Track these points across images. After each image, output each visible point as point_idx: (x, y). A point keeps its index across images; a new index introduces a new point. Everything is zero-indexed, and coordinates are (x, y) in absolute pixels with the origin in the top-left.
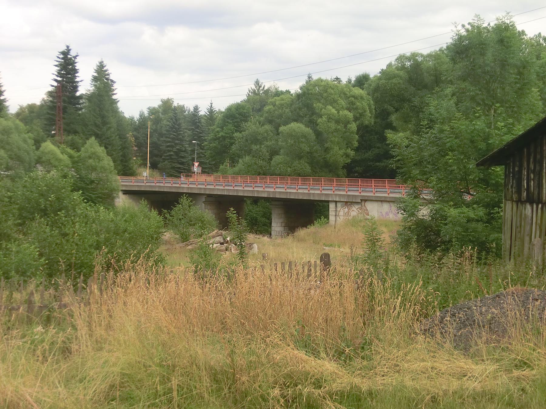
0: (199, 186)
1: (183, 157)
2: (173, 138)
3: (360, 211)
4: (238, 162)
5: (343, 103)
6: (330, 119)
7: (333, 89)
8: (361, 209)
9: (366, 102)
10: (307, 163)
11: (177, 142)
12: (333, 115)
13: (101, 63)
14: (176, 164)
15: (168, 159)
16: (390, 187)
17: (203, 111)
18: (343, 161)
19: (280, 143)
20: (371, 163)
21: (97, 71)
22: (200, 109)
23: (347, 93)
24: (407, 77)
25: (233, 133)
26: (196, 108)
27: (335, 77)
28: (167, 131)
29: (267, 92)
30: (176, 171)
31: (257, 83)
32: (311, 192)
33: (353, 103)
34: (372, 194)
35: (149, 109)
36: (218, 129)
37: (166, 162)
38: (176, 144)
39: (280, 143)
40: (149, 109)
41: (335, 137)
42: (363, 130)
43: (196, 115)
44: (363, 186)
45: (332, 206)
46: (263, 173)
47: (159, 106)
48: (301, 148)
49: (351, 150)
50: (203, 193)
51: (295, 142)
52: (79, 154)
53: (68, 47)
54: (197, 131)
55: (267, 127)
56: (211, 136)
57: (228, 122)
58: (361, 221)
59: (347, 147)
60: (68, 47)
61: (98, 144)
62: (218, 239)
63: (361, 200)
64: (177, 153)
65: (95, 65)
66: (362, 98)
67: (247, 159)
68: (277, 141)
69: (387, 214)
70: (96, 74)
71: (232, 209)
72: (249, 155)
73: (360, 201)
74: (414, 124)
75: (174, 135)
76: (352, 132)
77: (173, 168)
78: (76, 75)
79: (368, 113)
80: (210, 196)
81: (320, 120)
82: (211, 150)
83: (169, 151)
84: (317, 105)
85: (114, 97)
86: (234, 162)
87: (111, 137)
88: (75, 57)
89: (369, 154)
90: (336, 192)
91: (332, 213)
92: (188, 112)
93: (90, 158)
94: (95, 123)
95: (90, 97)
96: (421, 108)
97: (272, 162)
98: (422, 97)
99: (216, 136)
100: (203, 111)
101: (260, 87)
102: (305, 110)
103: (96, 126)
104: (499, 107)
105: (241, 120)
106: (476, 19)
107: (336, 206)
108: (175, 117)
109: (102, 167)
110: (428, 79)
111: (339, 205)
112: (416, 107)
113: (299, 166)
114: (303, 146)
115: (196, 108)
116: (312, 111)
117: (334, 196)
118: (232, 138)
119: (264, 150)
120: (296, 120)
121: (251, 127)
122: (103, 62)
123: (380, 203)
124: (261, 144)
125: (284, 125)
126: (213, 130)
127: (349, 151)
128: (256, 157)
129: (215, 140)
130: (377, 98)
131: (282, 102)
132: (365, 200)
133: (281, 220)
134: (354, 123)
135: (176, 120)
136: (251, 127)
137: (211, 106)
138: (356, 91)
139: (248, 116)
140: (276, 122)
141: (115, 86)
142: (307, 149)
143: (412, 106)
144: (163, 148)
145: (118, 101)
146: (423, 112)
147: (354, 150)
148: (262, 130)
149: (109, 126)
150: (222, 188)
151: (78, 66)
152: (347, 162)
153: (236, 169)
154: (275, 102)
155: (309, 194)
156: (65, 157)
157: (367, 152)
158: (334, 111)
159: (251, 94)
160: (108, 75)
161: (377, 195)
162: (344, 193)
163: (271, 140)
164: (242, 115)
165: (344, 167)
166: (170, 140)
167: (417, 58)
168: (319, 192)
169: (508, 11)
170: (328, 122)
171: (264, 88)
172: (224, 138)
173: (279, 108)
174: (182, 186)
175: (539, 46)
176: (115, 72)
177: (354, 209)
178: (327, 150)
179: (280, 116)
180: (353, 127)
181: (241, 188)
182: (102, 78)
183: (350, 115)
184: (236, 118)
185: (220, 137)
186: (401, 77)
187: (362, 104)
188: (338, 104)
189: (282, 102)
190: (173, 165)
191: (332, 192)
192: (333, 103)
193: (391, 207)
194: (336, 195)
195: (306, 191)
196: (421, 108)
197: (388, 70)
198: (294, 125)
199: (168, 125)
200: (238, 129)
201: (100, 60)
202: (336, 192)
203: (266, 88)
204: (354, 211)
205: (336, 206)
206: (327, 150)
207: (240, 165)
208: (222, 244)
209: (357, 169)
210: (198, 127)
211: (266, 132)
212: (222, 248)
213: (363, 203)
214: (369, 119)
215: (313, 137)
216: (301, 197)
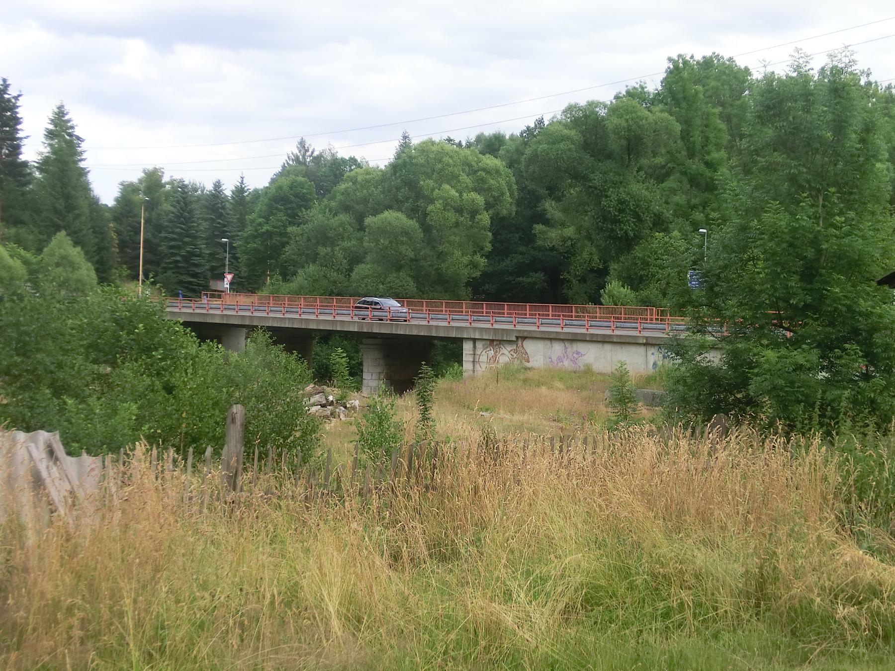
0: (241, 313)
1: (196, 265)
2: (180, 234)
3: (515, 355)
4: (295, 274)
5: (468, 181)
6: (446, 206)
7: (451, 157)
8: (516, 351)
9: (504, 182)
10: (410, 276)
11: (187, 239)
12: (452, 199)
13: (60, 108)
14: (184, 277)
15: (172, 268)
16: (473, 312)
17: (228, 191)
18: (465, 273)
19: (366, 244)
20: (511, 278)
21: (53, 121)
22: (223, 187)
23: (474, 164)
24: (582, 139)
25: (285, 227)
26: (218, 185)
27: (445, 138)
28: (170, 221)
29: (318, 159)
30: (185, 287)
31: (302, 144)
32: (432, 323)
33: (483, 180)
34: (534, 328)
35: (122, 184)
36: (261, 220)
37: (169, 273)
38: (187, 243)
39: (366, 244)
40: (122, 184)
41: (454, 234)
42: (500, 224)
43: (217, 197)
44: (433, 311)
45: (467, 347)
46: (334, 292)
47: (140, 181)
48: (400, 253)
49: (481, 257)
50: (247, 323)
51: (391, 242)
52: (39, 258)
53: (4, 80)
54: (219, 223)
55: (343, 217)
56: (249, 230)
57: (277, 209)
58: (518, 371)
59: (475, 252)
60: (4, 80)
61: (70, 242)
62: (317, 398)
63: (517, 338)
64: (187, 259)
65: (51, 111)
66: (498, 172)
67: (312, 268)
68: (361, 240)
69: (560, 360)
70: (51, 127)
71: (340, 350)
72: (314, 262)
73: (514, 339)
74: (593, 217)
75: (182, 228)
76: (484, 228)
77: (180, 283)
78: (19, 127)
79: (507, 197)
80: (270, 329)
81: (430, 208)
82: (247, 254)
83: (174, 255)
84: (426, 183)
85: (82, 165)
86: (286, 275)
87: (81, 230)
88: (16, 98)
89: (508, 263)
90: (474, 325)
91: (467, 357)
92: (202, 191)
93: (58, 265)
94: (54, 208)
95: (44, 165)
96: (605, 190)
97: (353, 275)
98: (605, 173)
99: (257, 231)
100: (228, 191)
101: (307, 151)
102: (405, 190)
103: (56, 211)
104: (834, 193)
105: (300, 207)
106: (796, 55)
107: (475, 347)
108: (184, 198)
109: (79, 281)
110: (615, 144)
111: (479, 345)
112: (596, 188)
113: (398, 281)
114: (403, 249)
115: (218, 185)
116: (418, 194)
117: (471, 331)
118: (283, 234)
119: (340, 255)
120: (389, 207)
121: (316, 215)
122: (62, 106)
123: (548, 342)
124: (333, 244)
125: (374, 215)
126: (253, 221)
127: (478, 258)
128: (326, 266)
129: (255, 237)
130: (534, 172)
131: (368, 177)
132: (523, 337)
133: (378, 370)
134: (485, 212)
135: (186, 204)
136: (316, 215)
137: (242, 183)
138: (488, 161)
139: (310, 200)
140: (359, 209)
141: (84, 146)
142: (411, 254)
143: (590, 187)
144: (163, 248)
145: (89, 172)
146: (607, 197)
147: (487, 257)
148: (335, 222)
149: (77, 212)
150: (281, 316)
151: (21, 113)
152: (474, 276)
153: (294, 285)
154: (356, 177)
155: (429, 327)
156: (16, 264)
157: (503, 260)
158: (454, 193)
159: (291, 163)
160: (72, 127)
161: (542, 329)
162: (488, 326)
163: (349, 239)
164: (299, 198)
165: (468, 284)
166: (175, 236)
167: (597, 109)
168: (445, 324)
169: (847, 44)
170: (444, 209)
171: (312, 153)
172: (270, 234)
173: (362, 186)
174: (211, 312)
175: (890, 100)
176: (83, 125)
177: (504, 351)
178: (441, 256)
179: (365, 201)
180: (485, 218)
181: (313, 317)
182: (61, 132)
183: (480, 199)
184: (291, 202)
185: (264, 233)
186: (573, 142)
187: (498, 182)
188: (459, 181)
189: (368, 177)
190: (181, 278)
191: (467, 325)
192: (453, 179)
193: (566, 348)
194: (475, 328)
195: (424, 323)
196: (605, 190)
197: (552, 129)
198: (389, 215)
199: (173, 213)
200: (294, 218)
201: (58, 104)
202: (474, 325)
203: (316, 154)
204: (505, 355)
205: (475, 347)
206: (441, 256)
207: (300, 279)
208: (323, 406)
209: (487, 286)
210: (220, 216)
211: (342, 225)
212: (325, 413)
213: (520, 342)
214: (508, 206)
215: (420, 234)
216: (415, 332)
